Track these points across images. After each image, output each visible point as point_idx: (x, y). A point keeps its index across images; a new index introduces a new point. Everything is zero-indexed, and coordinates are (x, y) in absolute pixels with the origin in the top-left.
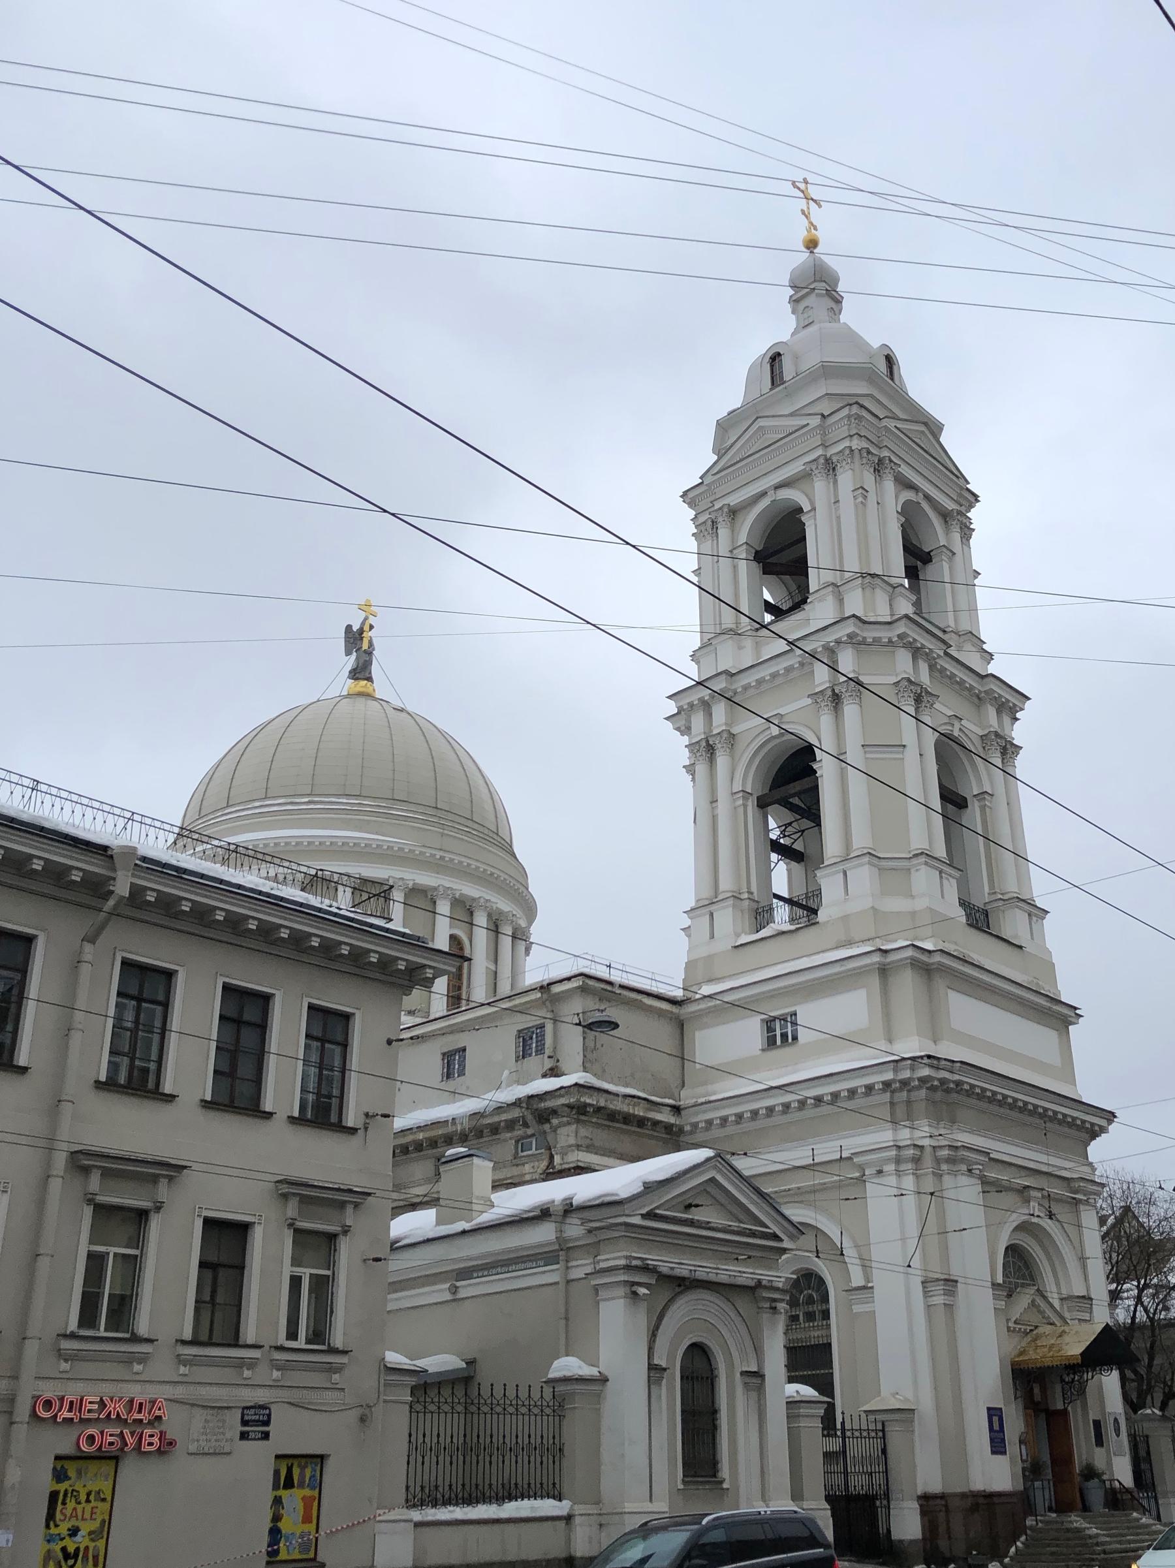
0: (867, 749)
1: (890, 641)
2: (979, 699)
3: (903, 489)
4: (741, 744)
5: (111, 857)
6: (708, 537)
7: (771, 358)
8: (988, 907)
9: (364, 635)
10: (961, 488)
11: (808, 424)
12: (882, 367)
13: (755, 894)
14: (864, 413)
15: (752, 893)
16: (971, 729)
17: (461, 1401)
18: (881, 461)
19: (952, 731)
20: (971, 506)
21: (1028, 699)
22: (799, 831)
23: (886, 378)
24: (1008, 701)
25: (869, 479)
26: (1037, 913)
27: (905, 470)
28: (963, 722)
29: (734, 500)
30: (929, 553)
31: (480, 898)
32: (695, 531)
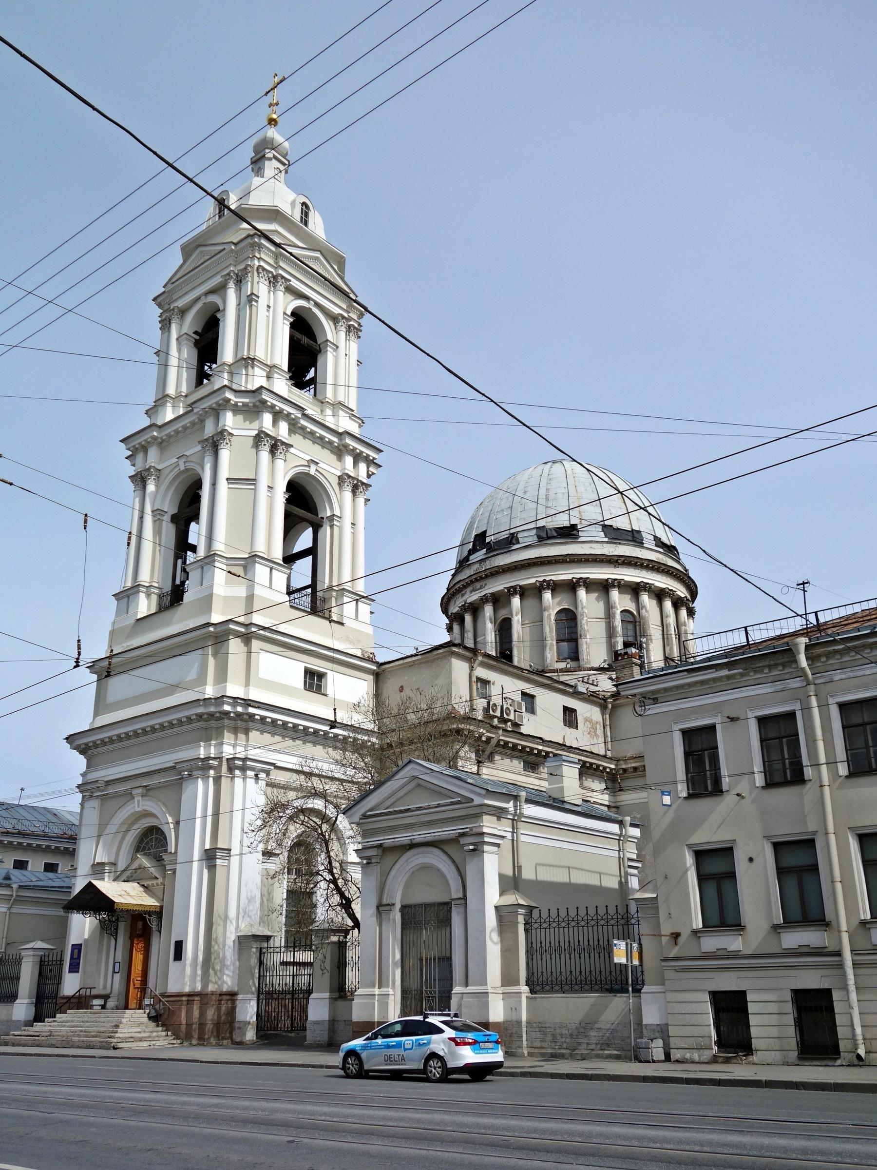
2: (340, 450)
3: (295, 299)
11: (224, 249)
17: (584, 919)
24: (361, 452)
27: (295, 283)
28: (319, 465)
29: (180, 303)
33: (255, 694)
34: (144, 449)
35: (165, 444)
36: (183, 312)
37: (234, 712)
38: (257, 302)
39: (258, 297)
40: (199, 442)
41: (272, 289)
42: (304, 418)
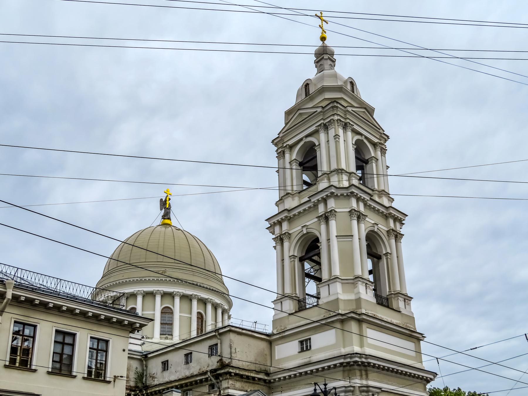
0: (338, 237)
1: (347, 195)
4: (293, 236)
5: (5, 284)
6: (282, 158)
7: (305, 86)
8: (388, 297)
9: (167, 202)
10: (381, 133)
11: (317, 111)
12: (349, 87)
13: (298, 294)
14: (339, 105)
15: (297, 294)
16: (382, 227)
18: (346, 124)
19: (374, 229)
20: (386, 141)
21: (407, 216)
22: (316, 270)
23: (350, 91)
24: (398, 217)
25: (341, 132)
26: (408, 299)
27: (356, 127)
28: (378, 226)
29: (290, 143)
30: (368, 160)
31: (208, 298)
32: (277, 155)
33: (368, 351)
34: (280, 223)
35: (291, 220)
36: (291, 147)
37: (361, 362)
38: (339, 139)
39: (339, 136)
40: (317, 218)
41: (345, 131)
42: (371, 200)
